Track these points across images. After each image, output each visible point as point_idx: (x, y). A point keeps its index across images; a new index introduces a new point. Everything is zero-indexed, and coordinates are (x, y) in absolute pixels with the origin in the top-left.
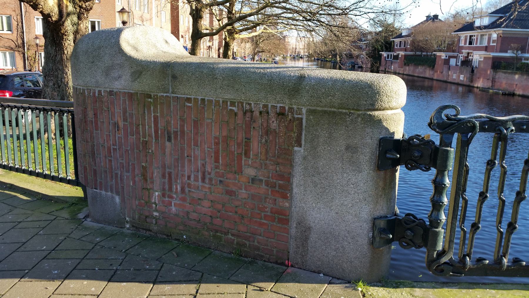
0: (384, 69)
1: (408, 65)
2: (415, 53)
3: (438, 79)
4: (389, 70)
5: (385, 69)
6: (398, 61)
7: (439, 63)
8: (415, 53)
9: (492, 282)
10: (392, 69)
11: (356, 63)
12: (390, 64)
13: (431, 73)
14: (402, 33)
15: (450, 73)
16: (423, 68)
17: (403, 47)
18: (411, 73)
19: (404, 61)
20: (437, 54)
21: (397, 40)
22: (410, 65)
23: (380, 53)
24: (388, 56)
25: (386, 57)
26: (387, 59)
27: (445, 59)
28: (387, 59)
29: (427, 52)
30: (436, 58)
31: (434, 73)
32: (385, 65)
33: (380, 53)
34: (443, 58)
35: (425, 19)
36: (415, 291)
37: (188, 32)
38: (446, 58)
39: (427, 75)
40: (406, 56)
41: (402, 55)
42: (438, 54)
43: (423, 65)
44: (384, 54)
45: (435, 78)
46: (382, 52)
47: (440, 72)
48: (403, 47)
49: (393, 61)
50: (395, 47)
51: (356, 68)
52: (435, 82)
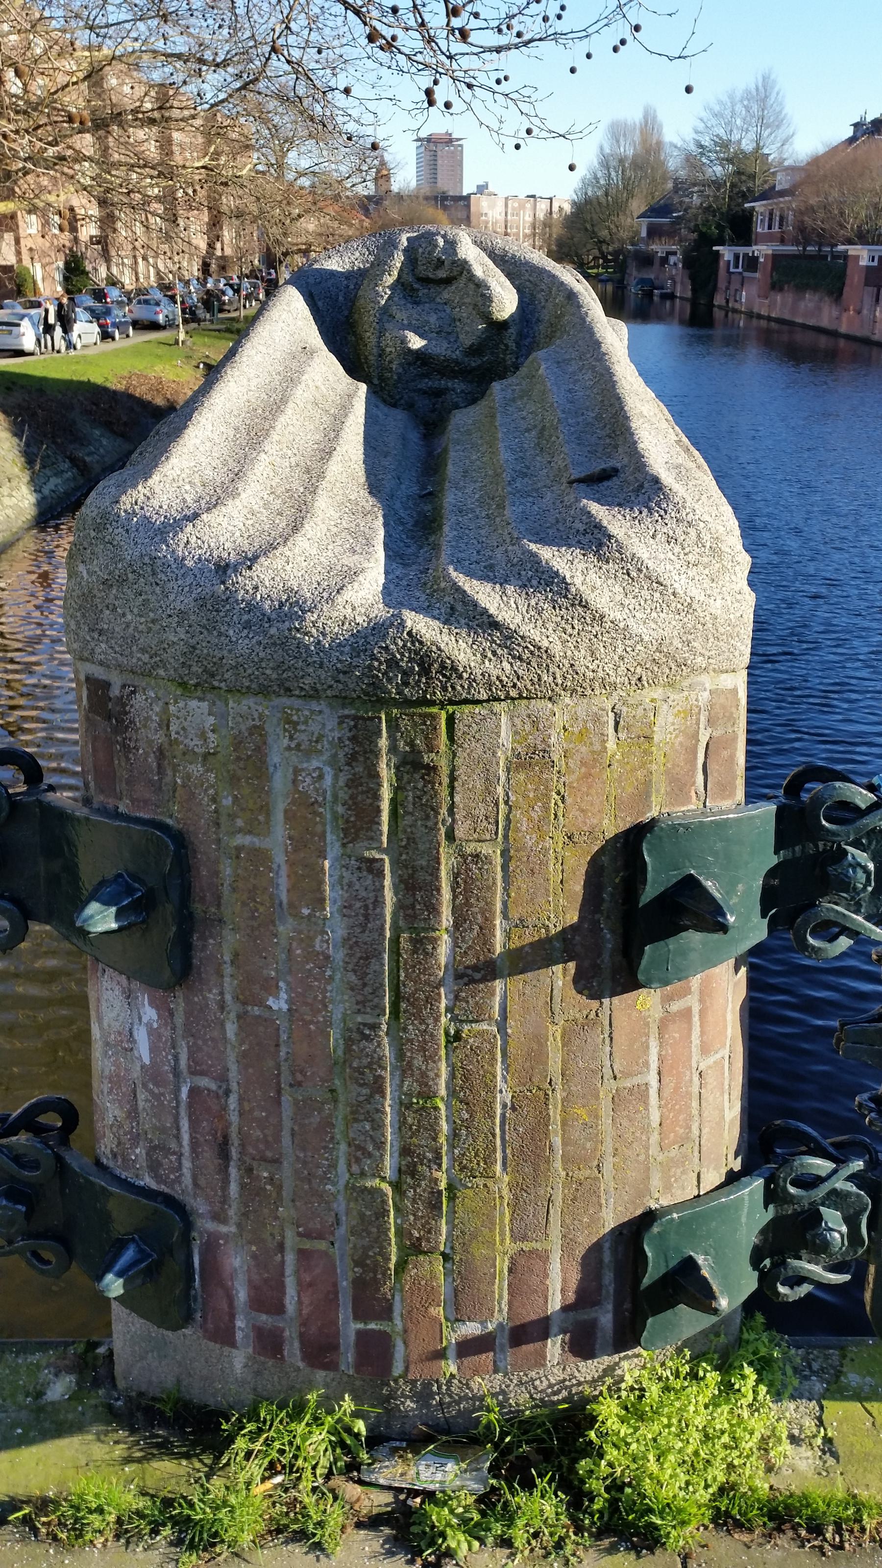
0: (723, 303)
1: (781, 290)
2: (805, 249)
3: (851, 333)
4: (737, 306)
5: (727, 301)
6: (757, 275)
7: (854, 279)
8: (805, 249)
9: (831, 978)
10: (743, 300)
11: (657, 283)
12: (738, 286)
13: (835, 313)
14: (774, 186)
15: (877, 314)
16: (817, 297)
17: (776, 229)
18: (787, 317)
19: (772, 276)
20: (850, 253)
21: (759, 206)
22: (786, 287)
23: (715, 248)
24: (737, 257)
25: (729, 262)
26: (732, 270)
27: (867, 267)
28: (732, 270)
29: (820, 245)
30: (845, 265)
31: (841, 315)
32: (727, 288)
33: (715, 248)
34: (864, 262)
35: (849, 132)
36: (737, 970)
37: (149, 216)
38: (871, 264)
39: (825, 322)
40: (776, 258)
41: (766, 256)
42: (853, 250)
43: (815, 288)
44: (726, 253)
45: (843, 329)
46: (722, 244)
47: (854, 310)
48: (776, 229)
49: (746, 274)
50: (759, 230)
51: (656, 299)
52: (842, 343)
